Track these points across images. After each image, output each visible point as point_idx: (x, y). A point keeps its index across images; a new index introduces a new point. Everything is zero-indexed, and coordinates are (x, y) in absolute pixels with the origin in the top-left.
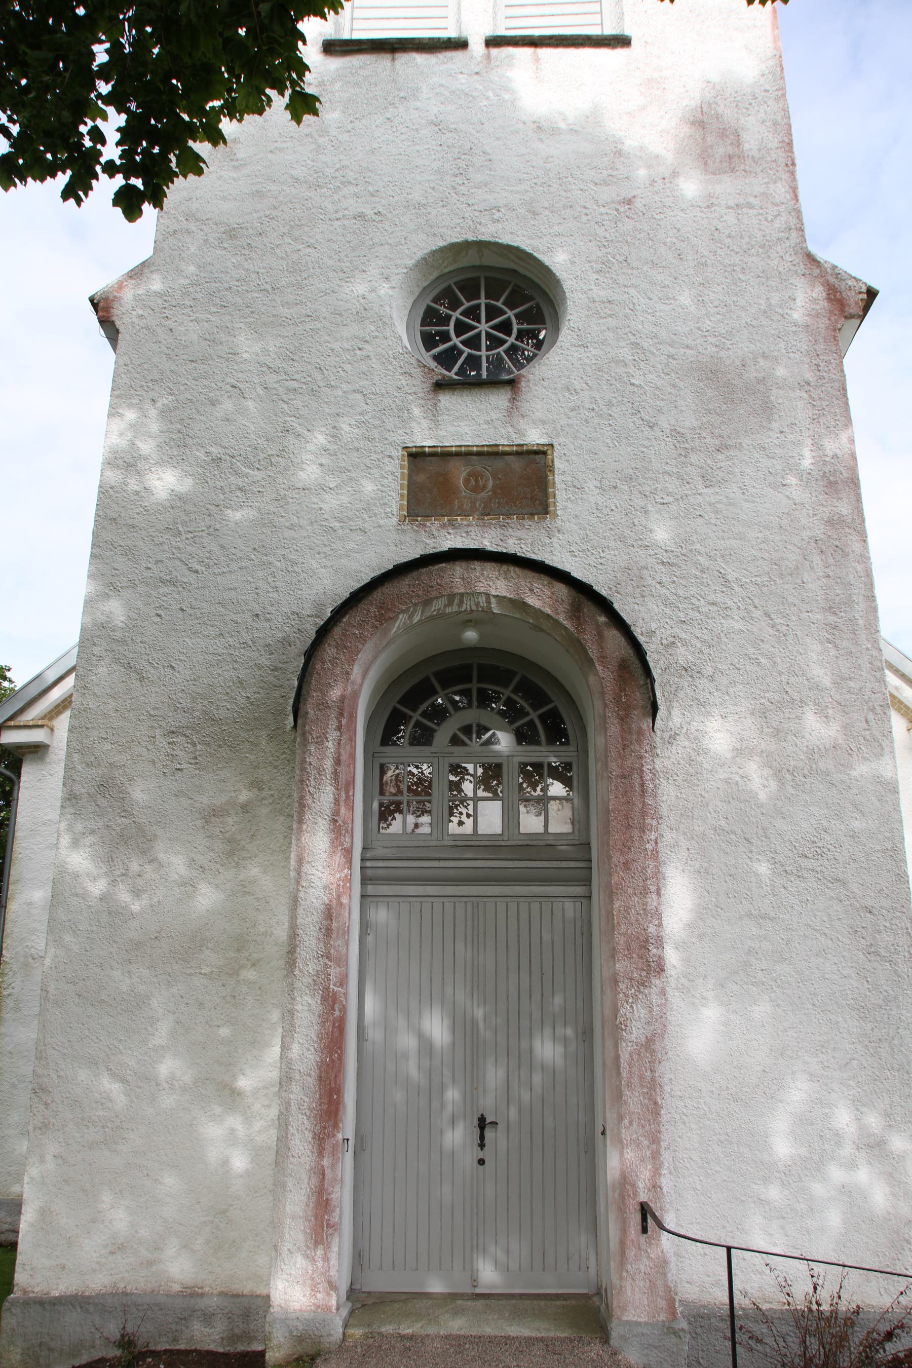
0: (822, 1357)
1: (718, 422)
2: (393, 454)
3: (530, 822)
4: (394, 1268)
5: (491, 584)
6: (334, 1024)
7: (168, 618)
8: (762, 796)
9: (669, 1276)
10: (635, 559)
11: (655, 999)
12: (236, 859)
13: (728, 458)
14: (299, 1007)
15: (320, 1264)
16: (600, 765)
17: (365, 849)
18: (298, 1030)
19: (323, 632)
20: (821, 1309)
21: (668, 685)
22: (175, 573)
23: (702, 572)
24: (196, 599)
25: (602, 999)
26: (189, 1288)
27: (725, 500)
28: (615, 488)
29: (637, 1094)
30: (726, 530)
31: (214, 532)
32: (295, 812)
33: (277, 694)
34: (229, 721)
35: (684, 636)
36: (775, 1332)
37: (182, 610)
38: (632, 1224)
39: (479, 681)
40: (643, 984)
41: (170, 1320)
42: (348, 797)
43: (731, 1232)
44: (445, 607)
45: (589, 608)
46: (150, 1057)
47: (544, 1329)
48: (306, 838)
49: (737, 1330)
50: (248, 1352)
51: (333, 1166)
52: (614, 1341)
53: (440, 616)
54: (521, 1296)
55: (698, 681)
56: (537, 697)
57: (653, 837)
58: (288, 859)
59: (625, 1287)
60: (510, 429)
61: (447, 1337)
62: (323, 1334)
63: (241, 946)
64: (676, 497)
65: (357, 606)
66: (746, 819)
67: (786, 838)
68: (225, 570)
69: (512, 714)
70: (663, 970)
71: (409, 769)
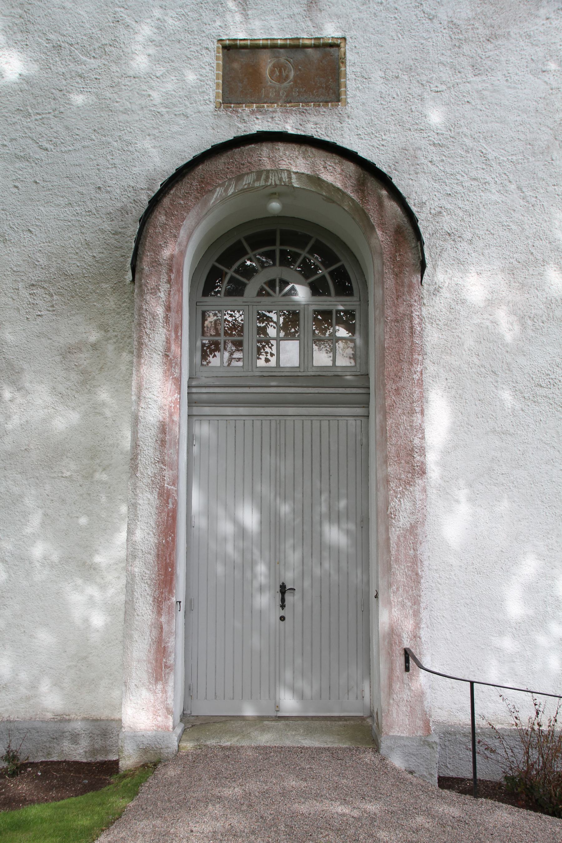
0: (541, 764)
1: (491, 12)
2: (209, 46)
3: (321, 358)
4: (216, 698)
5: (292, 162)
6: (168, 514)
7: (24, 189)
8: (509, 338)
9: (425, 703)
10: (411, 141)
11: (418, 495)
12: (88, 386)
13: (497, 47)
14: (140, 502)
15: (160, 695)
16: (378, 311)
17: (191, 378)
18: (140, 519)
19: (155, 202)
20: (541, 729)
21: (434, 248)
22: (28, 150)
23: (467, 151)
24: (47, 173)
25: (377, 494)
26: (59, 715)
27: (490, 87)
28: (397, 77)
29: (403, 567)
30: (489, 114)
31: (59, 115)
32: (138, 350)
33: (118, 254)
34: (79, 276)
35: (449, 206)
36: (505, 745)
37: (36, 182)
38: (398, 665)
39: (281, 244)
40: (409, 483)
41: (45, 740)
42: (177, 337)
43: (473, 672)
44: (254, 182)
45: (372, 183)
46: (24, 542)
47: (330, 742)
48: (144, 369)
49: (477, 744)
50: (106, 761)
51: (169, 622)
52: (383, 750)
53: (250, 189)
54: (313, 718)
55: (459, 244)
56: (329, 258)
57: (419, 369)
58: (130, 386)
59: (391, 710)
60: (310, 23)
61: (256, 748)
62: (163, 746)
63: (94, 454)
64: (448, 85)
65: (181, 180)
66: (494, 356)
67: (525, 372)
68: (70, 148)
69: (307, 272)
70: (424, 473)
71: (225, 317)
